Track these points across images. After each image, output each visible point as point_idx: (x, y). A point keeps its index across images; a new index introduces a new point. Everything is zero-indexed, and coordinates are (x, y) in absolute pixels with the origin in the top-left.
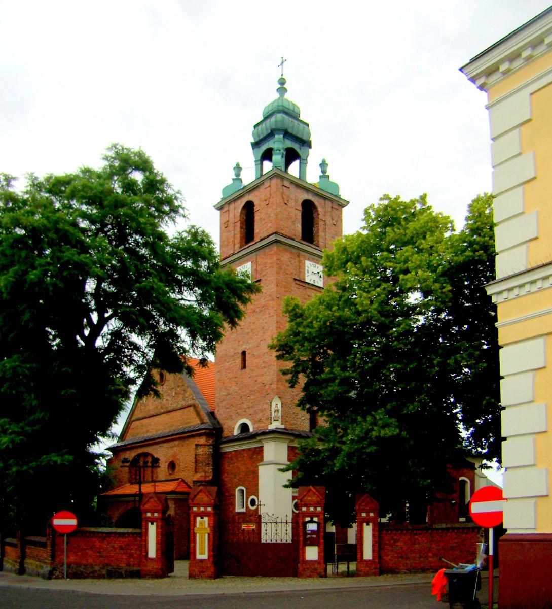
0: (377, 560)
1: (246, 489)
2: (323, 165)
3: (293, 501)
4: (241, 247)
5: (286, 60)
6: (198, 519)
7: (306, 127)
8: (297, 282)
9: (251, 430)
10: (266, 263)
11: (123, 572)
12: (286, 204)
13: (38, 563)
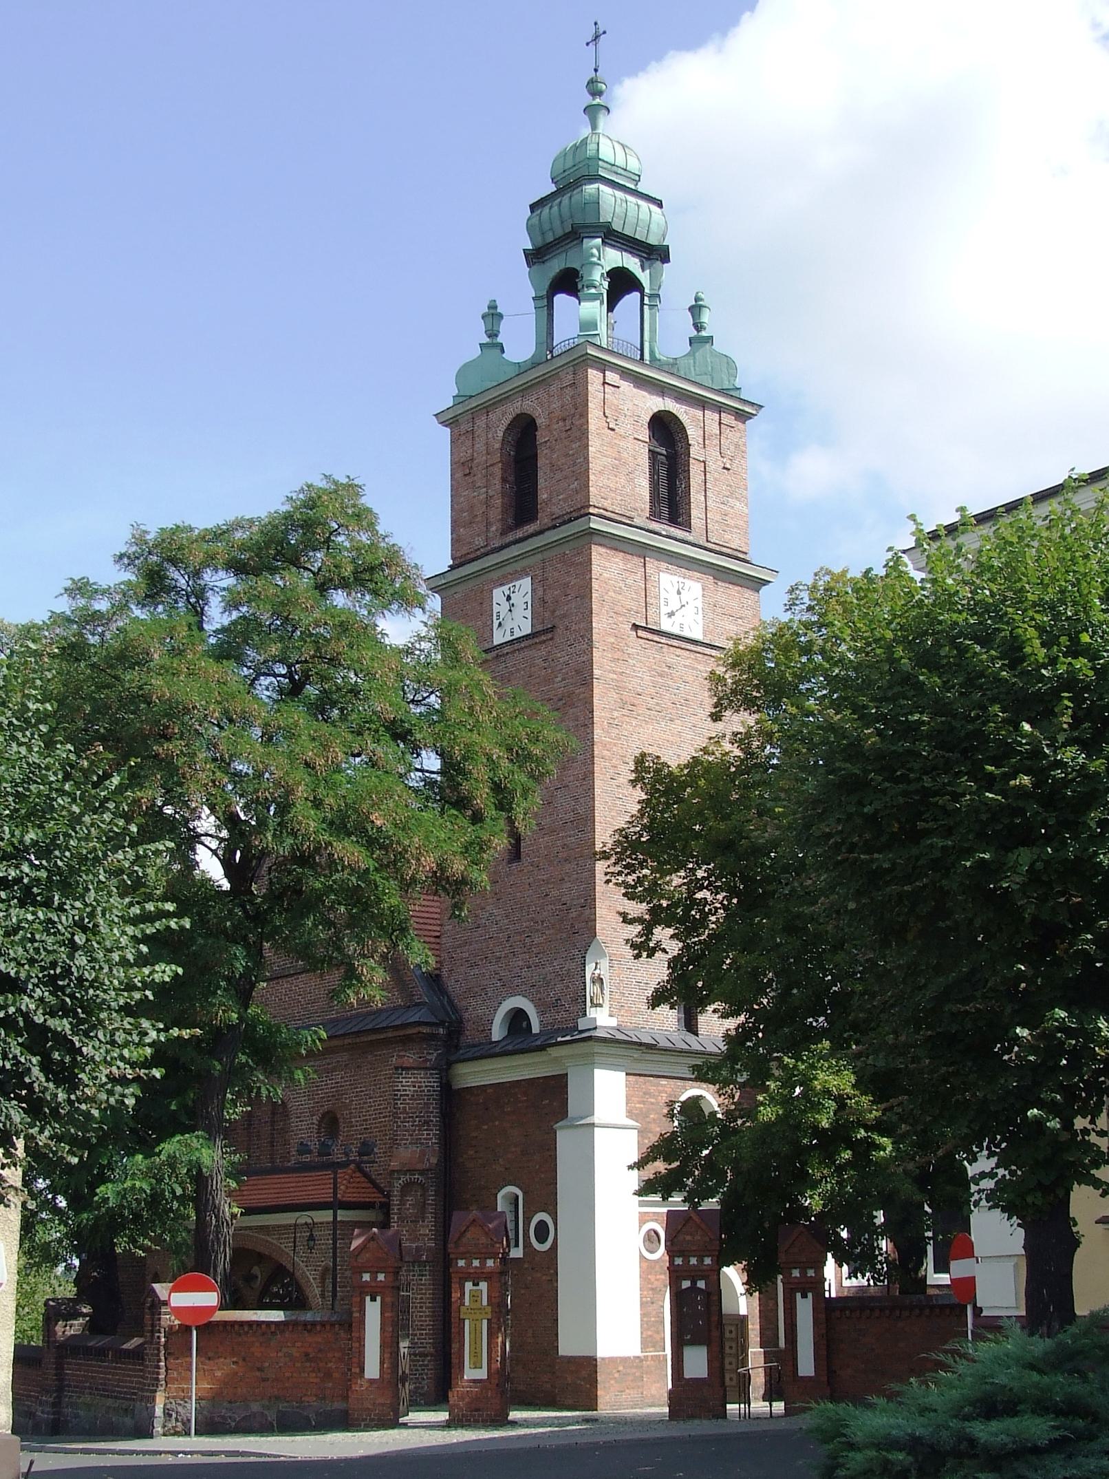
0: (825, 1379)
1: (525, 1193)
3: (640, 1227)
4: (504, 533)
5: (604, 33)
6: (469, 1286)
8: (640, 633)
9: (536, 1029)
10: (567, 585)
11: (312, 1416)
12: (613, 430)
13: (110, 1402)
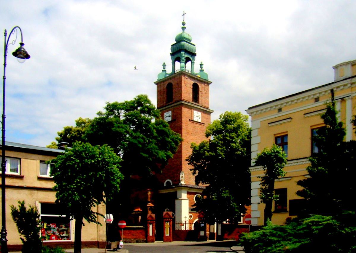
2: (201, 65)
4: (166, 103)
7: (194, 46)
8: (191, 121)
9: (172, 184)
10: (178, 112)
12: (186, 86)
